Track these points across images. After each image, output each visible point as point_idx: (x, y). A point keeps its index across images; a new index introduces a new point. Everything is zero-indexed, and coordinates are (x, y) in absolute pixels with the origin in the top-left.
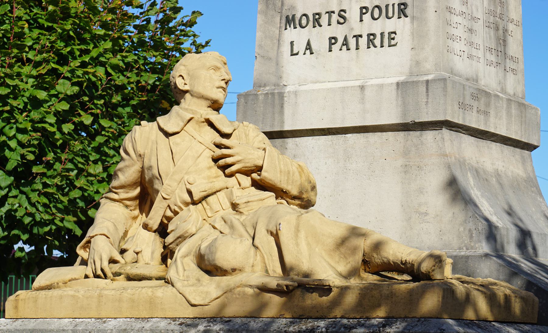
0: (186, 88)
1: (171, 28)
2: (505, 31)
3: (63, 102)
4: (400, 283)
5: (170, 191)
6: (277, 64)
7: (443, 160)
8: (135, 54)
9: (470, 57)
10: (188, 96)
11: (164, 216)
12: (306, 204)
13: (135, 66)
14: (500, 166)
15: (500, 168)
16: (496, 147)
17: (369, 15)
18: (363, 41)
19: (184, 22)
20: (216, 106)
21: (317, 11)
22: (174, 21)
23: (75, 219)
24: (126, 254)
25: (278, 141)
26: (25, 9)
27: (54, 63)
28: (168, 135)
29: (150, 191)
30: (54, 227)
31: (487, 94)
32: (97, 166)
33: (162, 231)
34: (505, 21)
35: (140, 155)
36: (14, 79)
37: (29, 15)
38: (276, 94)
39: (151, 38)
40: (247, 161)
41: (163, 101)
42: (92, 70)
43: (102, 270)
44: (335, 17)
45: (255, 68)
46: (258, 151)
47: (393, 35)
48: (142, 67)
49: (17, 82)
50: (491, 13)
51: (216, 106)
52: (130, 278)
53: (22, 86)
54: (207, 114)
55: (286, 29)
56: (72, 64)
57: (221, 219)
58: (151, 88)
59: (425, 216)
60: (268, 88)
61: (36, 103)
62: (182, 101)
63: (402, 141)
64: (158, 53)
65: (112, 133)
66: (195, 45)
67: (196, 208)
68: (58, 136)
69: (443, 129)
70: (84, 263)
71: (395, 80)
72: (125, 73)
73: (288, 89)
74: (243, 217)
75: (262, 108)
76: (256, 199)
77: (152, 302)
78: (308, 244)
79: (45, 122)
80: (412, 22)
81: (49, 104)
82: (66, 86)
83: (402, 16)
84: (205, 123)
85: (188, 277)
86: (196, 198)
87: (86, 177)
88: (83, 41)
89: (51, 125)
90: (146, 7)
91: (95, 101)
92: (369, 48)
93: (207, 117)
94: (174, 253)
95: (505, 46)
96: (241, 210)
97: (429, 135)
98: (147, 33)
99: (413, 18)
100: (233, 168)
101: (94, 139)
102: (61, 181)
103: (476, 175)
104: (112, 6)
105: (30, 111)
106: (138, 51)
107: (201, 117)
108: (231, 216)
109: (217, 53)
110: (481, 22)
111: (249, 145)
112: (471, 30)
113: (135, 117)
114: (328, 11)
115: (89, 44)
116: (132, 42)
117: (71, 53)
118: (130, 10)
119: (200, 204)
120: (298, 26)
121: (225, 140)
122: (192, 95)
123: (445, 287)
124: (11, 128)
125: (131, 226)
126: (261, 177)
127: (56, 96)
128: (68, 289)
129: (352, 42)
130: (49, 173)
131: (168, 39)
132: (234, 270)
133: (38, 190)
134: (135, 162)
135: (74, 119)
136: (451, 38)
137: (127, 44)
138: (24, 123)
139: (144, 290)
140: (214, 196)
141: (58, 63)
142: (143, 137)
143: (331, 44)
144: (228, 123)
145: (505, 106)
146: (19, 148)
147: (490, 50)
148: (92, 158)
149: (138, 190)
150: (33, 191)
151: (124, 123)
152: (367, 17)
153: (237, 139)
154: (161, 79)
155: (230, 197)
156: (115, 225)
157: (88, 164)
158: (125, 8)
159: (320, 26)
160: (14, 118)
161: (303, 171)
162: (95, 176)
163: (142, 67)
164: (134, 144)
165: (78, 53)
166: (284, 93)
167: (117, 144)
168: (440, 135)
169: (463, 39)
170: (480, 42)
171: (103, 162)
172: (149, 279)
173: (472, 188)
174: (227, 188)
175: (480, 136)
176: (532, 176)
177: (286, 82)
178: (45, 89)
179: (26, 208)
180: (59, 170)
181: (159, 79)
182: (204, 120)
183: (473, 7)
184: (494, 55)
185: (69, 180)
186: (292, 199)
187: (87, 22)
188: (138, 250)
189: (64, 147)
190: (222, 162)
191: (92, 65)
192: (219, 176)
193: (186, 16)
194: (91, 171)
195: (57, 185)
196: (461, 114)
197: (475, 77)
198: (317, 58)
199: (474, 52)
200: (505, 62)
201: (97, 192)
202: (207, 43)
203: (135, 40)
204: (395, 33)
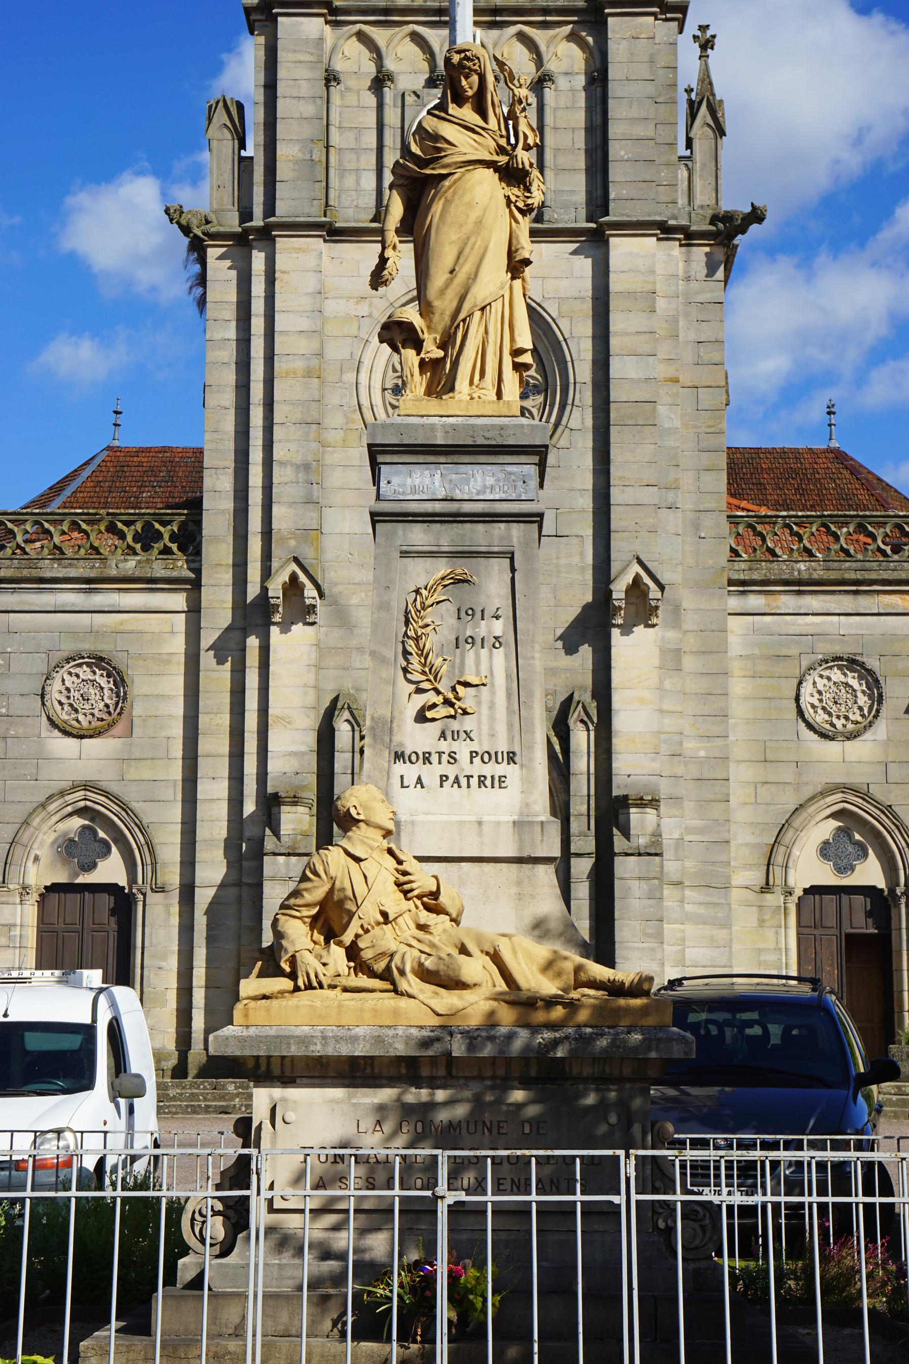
0: (361, 817)
10: (362, 824)
17: (479, 757)
18: (474, 781)
21: (428, 750)
44: (445, 758)
47: (503, 779)
52: (345, 990)
71: (511, 819)
77: (396, 1012)
99: (522, 766)
120: (407, 761)
122: (367, 824)
129: (463, 782)
132: (475, 985)
139: (386, 1001)
143: (442, 781)
152: (477, 760)
159: (431, 763)
190: (406, 887)
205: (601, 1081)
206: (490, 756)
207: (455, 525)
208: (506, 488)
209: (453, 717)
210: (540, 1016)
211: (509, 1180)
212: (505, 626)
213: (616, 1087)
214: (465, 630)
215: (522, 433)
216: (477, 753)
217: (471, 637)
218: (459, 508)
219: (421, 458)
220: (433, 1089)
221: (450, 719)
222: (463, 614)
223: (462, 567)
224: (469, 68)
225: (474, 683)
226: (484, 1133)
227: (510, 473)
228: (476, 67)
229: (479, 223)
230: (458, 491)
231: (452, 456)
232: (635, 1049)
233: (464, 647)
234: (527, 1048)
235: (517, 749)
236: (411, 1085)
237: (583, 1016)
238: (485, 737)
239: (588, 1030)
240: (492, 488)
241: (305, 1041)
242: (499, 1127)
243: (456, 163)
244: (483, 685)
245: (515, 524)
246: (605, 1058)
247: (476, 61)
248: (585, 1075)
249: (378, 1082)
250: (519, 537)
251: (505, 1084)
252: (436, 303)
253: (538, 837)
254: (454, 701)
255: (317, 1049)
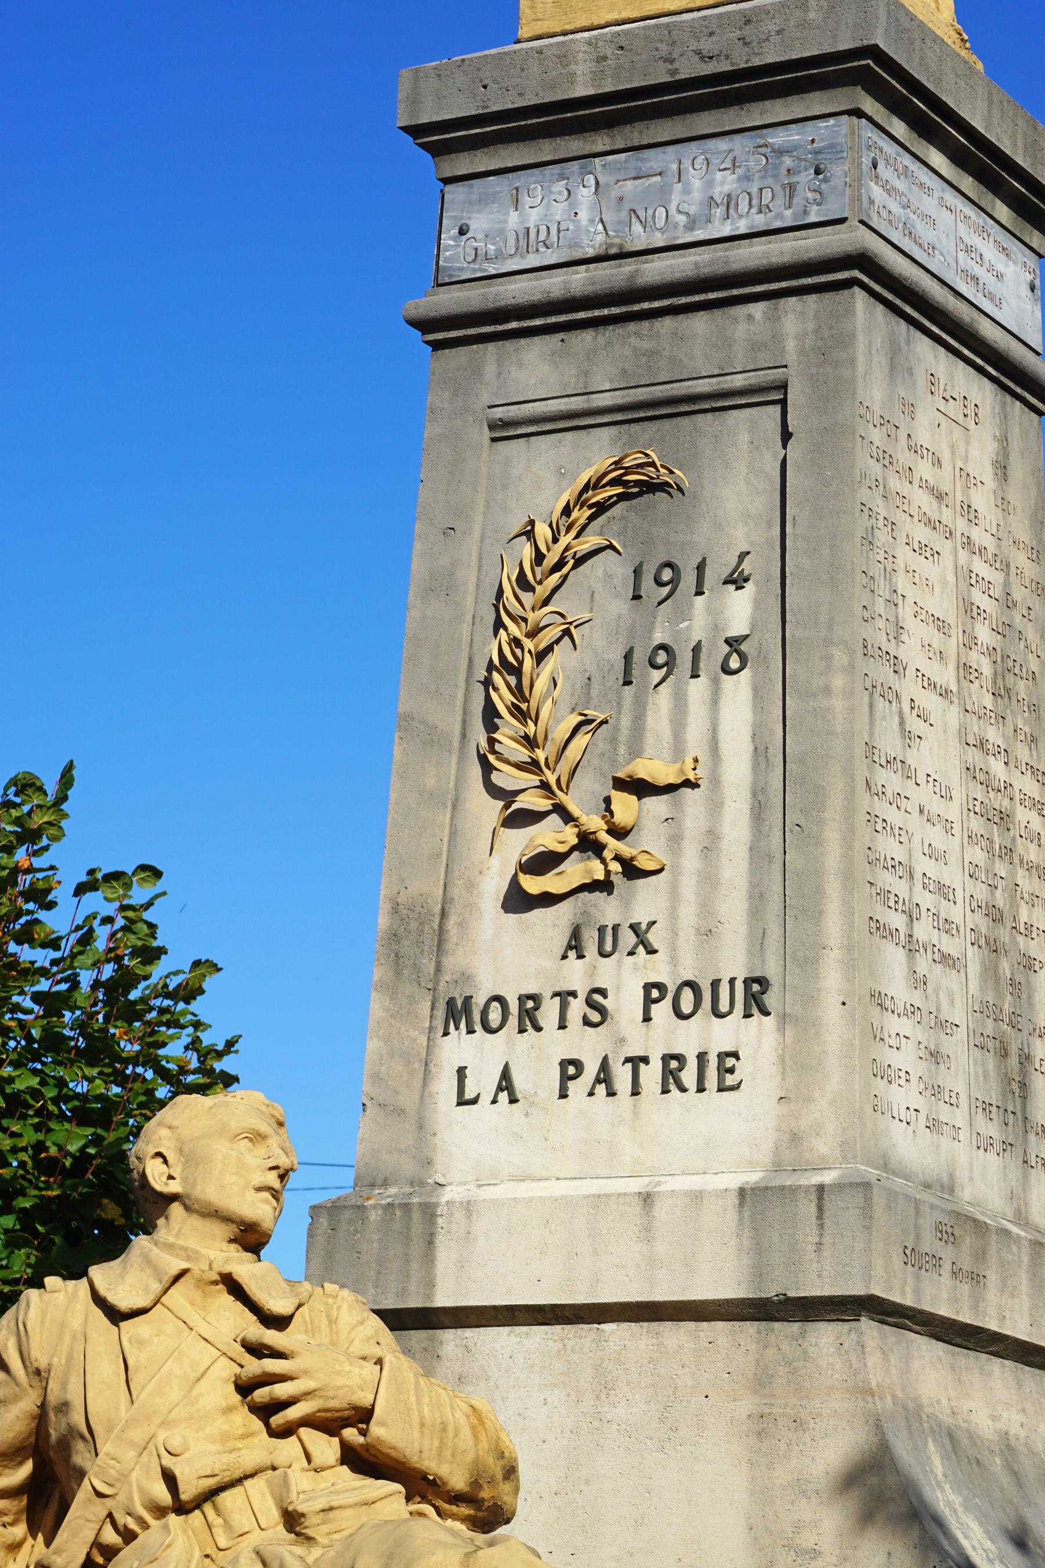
0: (174, 1187)
1: (135, 1003)
2: (1026, 1058)
6: (421, 1127)
7: (862, 1404)
8: (35, 1072)
9: (934, 1125)
10: (176, 1209)
13: (32, 1102)
14: (1013, 1422)
15: (1014, 1429)
17: (667, 1004)
18: (651, 1075)
19: (171, 988)
20: (252, 1238)
21: (532, 990)
22: (142, 985)
25: (417, 1337)
28: (116, 1316)
29: (60, 1470)
31: (979, 1227)
34: (1025, 1032)
35: (38, 1372)
38: (415, 1209)
39: (81, 1026)
40: (331, 1393)
41: (106, 1201)
44: (577, 1008)
45: (360, 1135)
46: (362, 1367)
47: (730, 1062)
48: (51, 1107)
50: (987, 1010)
51: (251, 1238)
54: (227, 1261)
55: (446, 1034)
57: (254, 1556)
58: (72, 1165)
59: (812, 1559)
60: (392, 1190)
62: (161, 1222)
63: (752, 1347)
64: (94, 1072)
66: (197, 1050)
67: (186, 1522)
69: (863, 1319)
71: (734, 1181)
73: (448, 1195)
74: (316, 1552)
75: (375, 1245)
76: (351, 1500)
80: (781, 1029)
83: (755, 1011)
84: (221, 1286)
86: (187, 1493)
92: (665, 1091)
93: (227, 1269)
95: (1024, 1098)
96: (309, 1532)
97: (825, 1335)
98: (68, 1015)
99: (784, 1018)
100: (293, 1413)
103: (949, 1448)
106: (44, 1064)
107: (211, 1269)
108: (281, 1549)
109: (260, 1096)
110: (961, 1034)
111: (338, 1349)
112: (935, 1056)
113: (26, 1244)
114: (558, 989)
116: (29, 1038)
118: (27, 954)
119: (197, 1512)
120: (478, 1027)
121: (272, 1333)
122: (187, 1208)
126: (368, 1439)
129: (622, 1076)
131: (125, 1033)
134: (24, 1390)
136: (884, 1073)
137: (12, 1044)
140: (237, 1491)
143: (565, 1079)
144: (284, 1285)
145: (1026, 1259)
147: (986, 1107)
152: (662, 1011)
153: (306, 1332)
154: (103, 1138)
159: (539, 1029)
161: (483, 1424)
163: (51, 1107)
164: (24, 1339)
166: (437, 1205)
168: (854, 1336)
169: (914, 1078)
170: (960, 1087)
173: (938, 1483)
174: (274, 1468)
175: (959, 1341)
177: (444, 1175)
181: (97, 1141)
182: (217, 1277)
183: (941, 994)
184: (995, 1121)
186: (450, 1503)
190: (261, 1395)
192: (251, 1435)
193: (176, 973)
196: (910, 1280)
197: (946, 1180)
198: (527, 1115)
199: (945, 1114)
200: (1026, 1141)
202: (230, 1044)
206: (695, 997)
207: (632, 326)
209: (605, 886)
212: (758, 604)
214: (650, 631)
216: (660, 986)
223: (650, 446)
225: (662, 780)
227: (780, 152)
230: (637, 228)
235: (772, 970)
238: (687, 940)
240: (730, 202)
244: (688, 784)
250: (801, 337)
254: (604, 837)
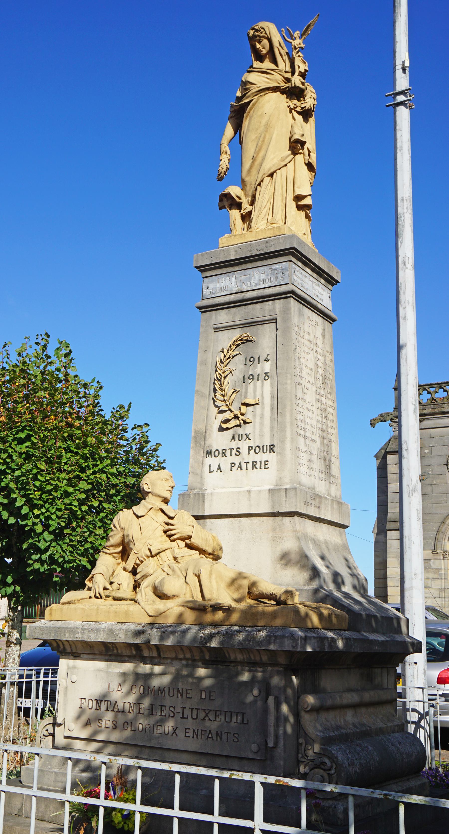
0: (149, 490)
2: (330, 461)
3: (82, 494)
4: (269, 606)
5: (139, 549)
6: (201, 477)
8: (124, 467)
9: (310, 475)
10: (150, 495)
11: (135, 563)
12: (216, 558)
14: (327, 537)
15: (328, 539)
16: (325, 527)
18: (250, 466)
20: (166, 501)
23: (87, 560)
24: (113, 585)
25: (202, 521)
26: (63, 442)
27: (78, 471)
28: (138, 517)
29: (127, 548)
30: (75, 564)
31: (320, 497)
32: (100, 530)
33: (134, 572)
35: (122, 528)
36: (56, 481)
37: (65, 445)
42: (99, 476)
43: (99, 594)
47: (267, 463)
48: (127, 474)
49: (57, 482)
51: (166, 501)
52: (115, 599)
53: (60, 484)
54: (161, 505)
56: (88, 472)
60: (196, 491)
61: (67, 494)
62: (147, 497)
64: (136, 467)
65: (109, 511)
68: (79, 513)
70: (90, 589)
72: (118, 477)
73: (207, 492)
74: (180, 565)
77: (127, 613)
78: (217, 582)
79: (72, 505)
81: (74, 495)
82: (84, 485)
83: (272, 452)
84: (160, 511)
85: (148, 599)
87: (94, 536)
88: (95, 460)
89: (75, 506)
90: (130, 440)
91: (101, 493)
92: (253, 469)
93: (161, 507)
94: (140, 585)
95: (330, 469)
97: (287, 520)
99: (278, 453)
100: (175, 537)
101: (99, 514)
102: (80, 539)
104: (111, 440)
105: (64, 499)
110: (316, 456)
111: (184, 524)
112: (310, 461)
113: (123, 502)
115: (98, 461)
116: (122, 459)
117: (88, 466)
118: (122, 442)
120: (213, 456)
122: (152, 495)
123: (295, 609)
124: (53, 508)
125: (116, 568)
127: (79, 490)
128: (80, 604)
129: (244, 466)
130: (74, 534)
132: (174, 596)
133: (67, 543)
135: (89, 503)
136: (299, 464)
138: (60, 505)
139: (122, 606)
141: (79, 472)
142: (124, 518)
143: (232, 467)
145: (330, 503)
146: (57, 519)
147: (322, 471)
148: (98, 525)
149: (121, 548)
150: (64, 543)
151: (116, 505)
152: (252, 452)
155: (173, 553)
156: (107, 568)
157: (96, 529)
158: (119, 441)
159: (226, 456)
160: (55, 502)
162: (99, 535)
163: (127, 474)
165: (91, 466)
167: (112, 517)
169: (306, 466)
171: (104, 527)
172: (126, 600)
176: (345, 543)
178: (73, 487)
179: (60, 553)
180: (79, 532)
181: (137, 481)
185: (85, 537)
187: (97, 449)
188: (119, 583)
189: (82, 518)
190: (168, 533)
191: (99, 473)
194: (97, 533)
195: (78, 541)
196: (305, 508)
199: (312, 473)
200: (330, 478)
201: (100, 545)
203: (124, 459)
204: (268, 461)
205: (252, 665)
206: (259, 449)
207: (244, 307)
208: (272, 279)
209: (239, 426)
210: (209, 618)
211: (192, 730)
212: (271, 365)
213: (261, 669)
214: (248, 371)
215: (279, 243)
217: (251, 375)
218: (244, 296)
219: (225, 270)
220: (153, 665)
221: (238, 428)
222: (248, 361)
223: (248, 332)
224: (259, 36)
225: (251, 403)
226: (178, 697)
227: (274, 270)
228: (264, 34)
229: (267, 126)
230: (244, 286)
231: (242, 265)
232: (260, 643)
233: (248, 382)
234: (194, 639)
235: (275, 443)
236: (141, 662)
237: (235, 617)
238: (257, 437)
239: (236, 628)
240: (264, 280)
241: (73, 631)
242: (187, 693)
243: (253, 93)
244: (257, 404)
245: (278, 301)
246: (243, 648)
247: (262, 30)
248: (239, 660)
249: (123, 659)
251: (193, 664)
252: (247, 179)
253: (283, 498)
254: (239, 415)
255: (79, 637)
